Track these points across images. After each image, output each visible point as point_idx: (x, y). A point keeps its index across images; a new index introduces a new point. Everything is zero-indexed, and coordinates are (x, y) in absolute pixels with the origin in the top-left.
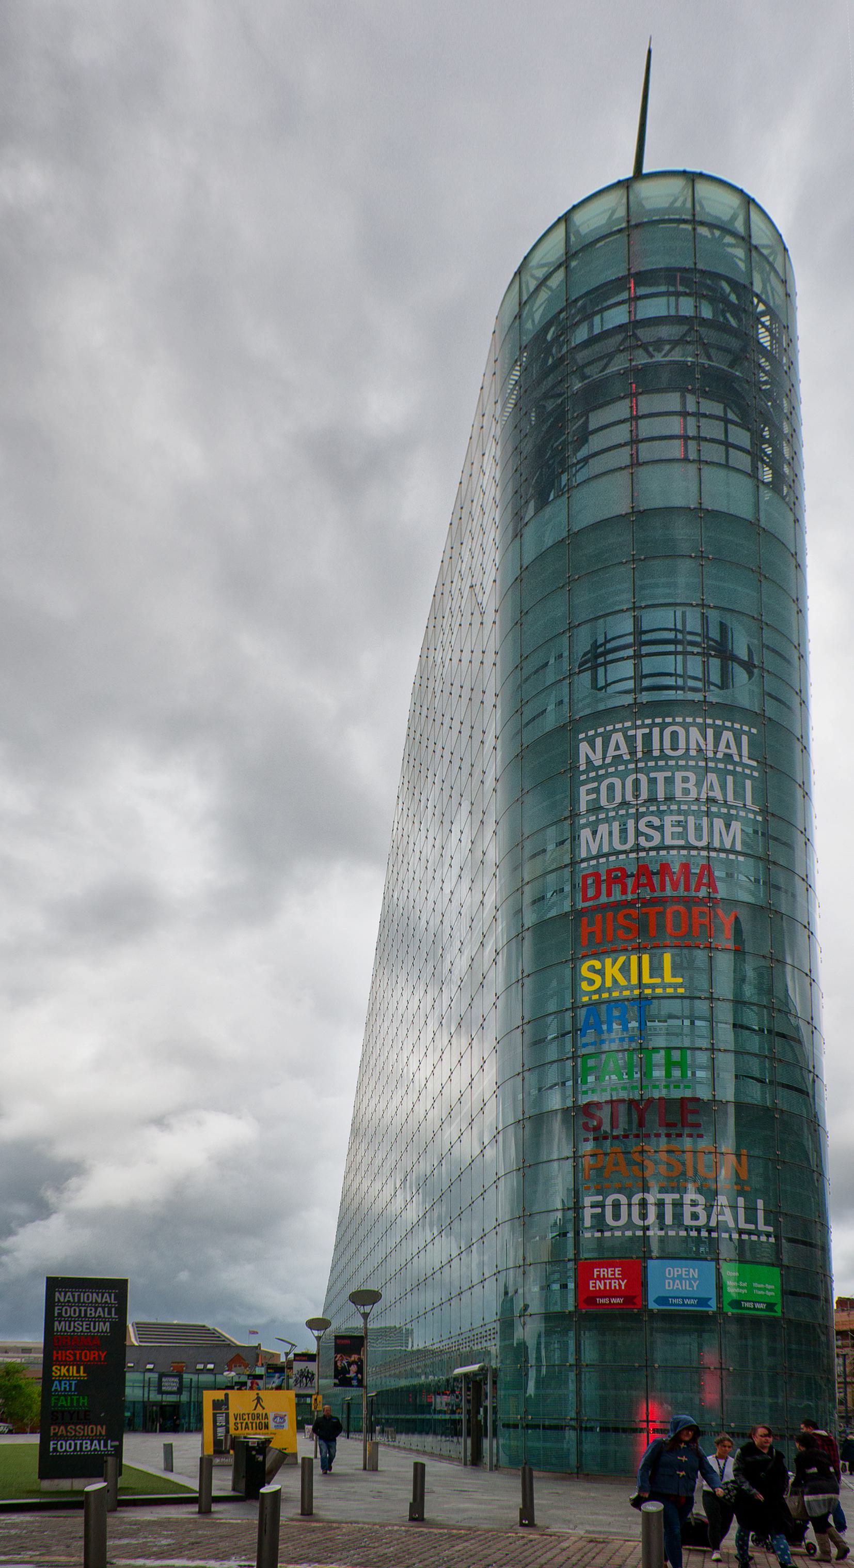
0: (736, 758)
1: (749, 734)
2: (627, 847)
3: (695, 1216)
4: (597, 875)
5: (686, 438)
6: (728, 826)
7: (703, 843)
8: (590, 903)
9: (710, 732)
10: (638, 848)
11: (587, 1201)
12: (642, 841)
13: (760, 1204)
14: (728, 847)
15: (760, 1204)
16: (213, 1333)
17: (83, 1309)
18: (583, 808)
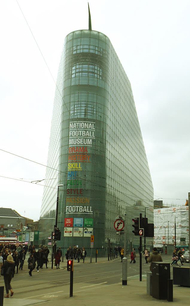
0: (92, 128)
1: (94, 124)
2: (75, 144)
3: (81, 210)
4: (71, 148)
5: (92, 107)
6: (90, 140)
7: (86, 144)
8: (70, 153)
9: (88, 124)
10: (77, 144)
11: (67, 207)
12: (78, 143)
13: (91, 207)
14: (89, 144)
15: (91, 207)
16: (13, 212)
17: (80, 131)
18: (70, 136)
